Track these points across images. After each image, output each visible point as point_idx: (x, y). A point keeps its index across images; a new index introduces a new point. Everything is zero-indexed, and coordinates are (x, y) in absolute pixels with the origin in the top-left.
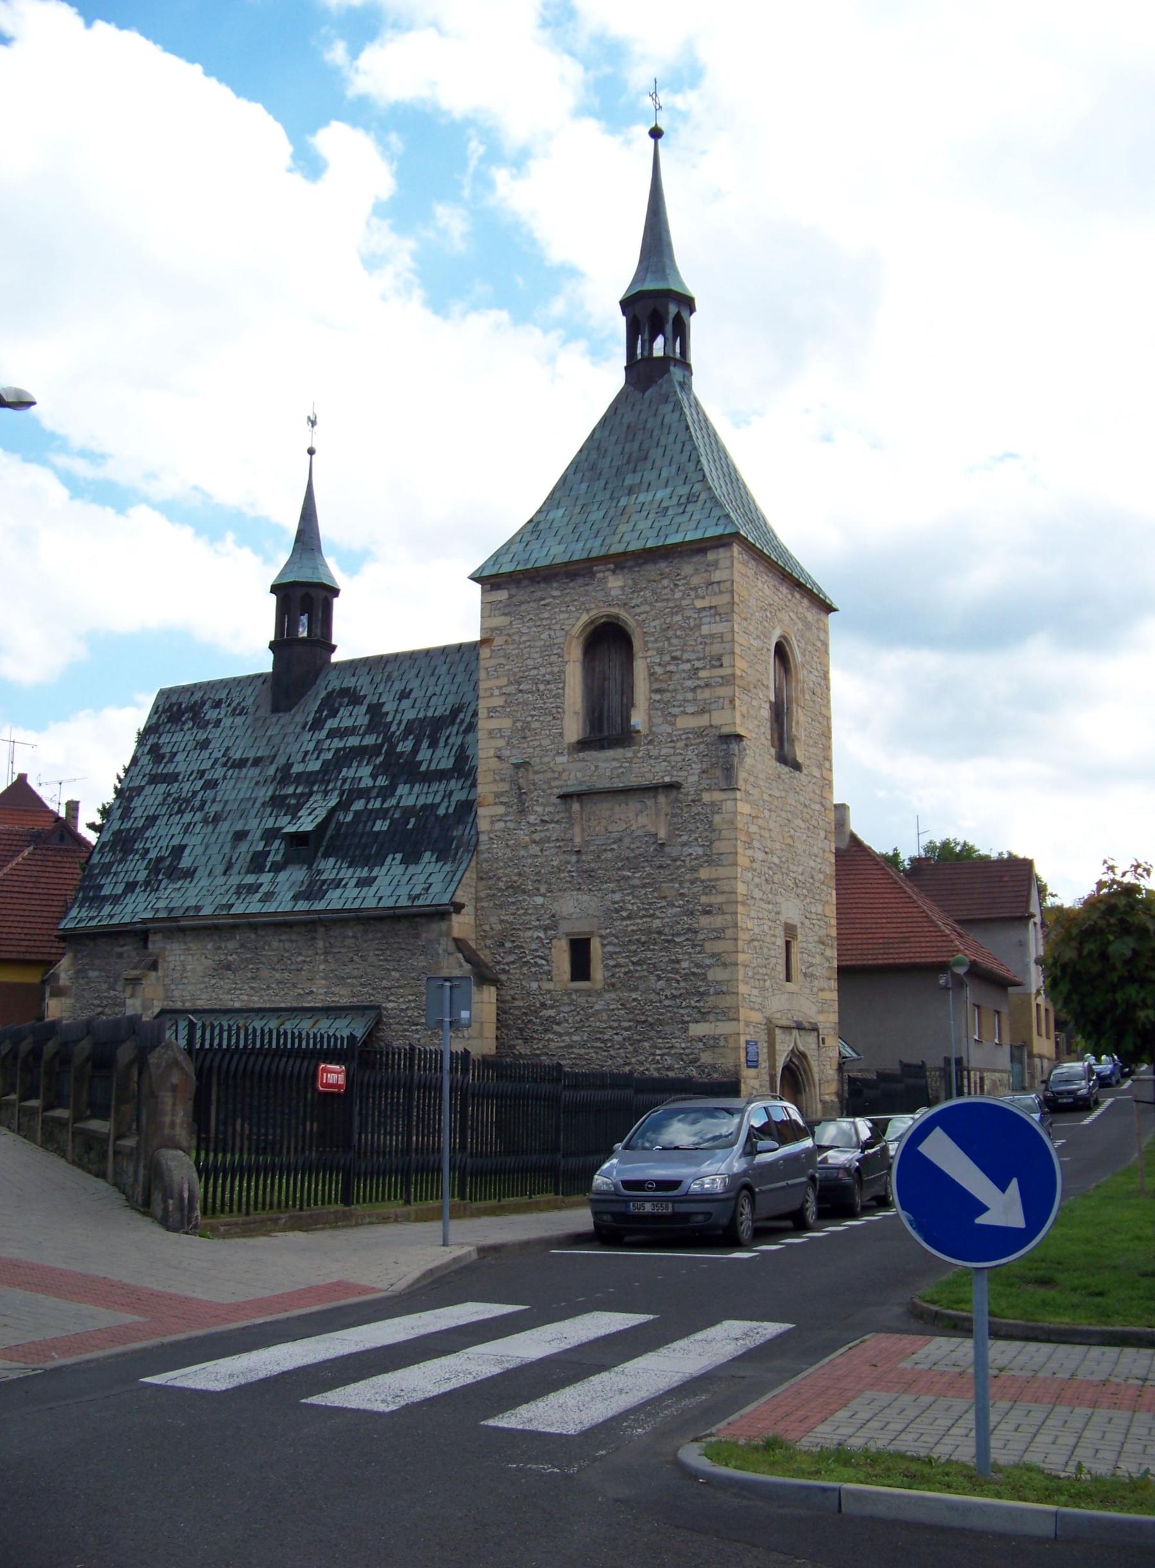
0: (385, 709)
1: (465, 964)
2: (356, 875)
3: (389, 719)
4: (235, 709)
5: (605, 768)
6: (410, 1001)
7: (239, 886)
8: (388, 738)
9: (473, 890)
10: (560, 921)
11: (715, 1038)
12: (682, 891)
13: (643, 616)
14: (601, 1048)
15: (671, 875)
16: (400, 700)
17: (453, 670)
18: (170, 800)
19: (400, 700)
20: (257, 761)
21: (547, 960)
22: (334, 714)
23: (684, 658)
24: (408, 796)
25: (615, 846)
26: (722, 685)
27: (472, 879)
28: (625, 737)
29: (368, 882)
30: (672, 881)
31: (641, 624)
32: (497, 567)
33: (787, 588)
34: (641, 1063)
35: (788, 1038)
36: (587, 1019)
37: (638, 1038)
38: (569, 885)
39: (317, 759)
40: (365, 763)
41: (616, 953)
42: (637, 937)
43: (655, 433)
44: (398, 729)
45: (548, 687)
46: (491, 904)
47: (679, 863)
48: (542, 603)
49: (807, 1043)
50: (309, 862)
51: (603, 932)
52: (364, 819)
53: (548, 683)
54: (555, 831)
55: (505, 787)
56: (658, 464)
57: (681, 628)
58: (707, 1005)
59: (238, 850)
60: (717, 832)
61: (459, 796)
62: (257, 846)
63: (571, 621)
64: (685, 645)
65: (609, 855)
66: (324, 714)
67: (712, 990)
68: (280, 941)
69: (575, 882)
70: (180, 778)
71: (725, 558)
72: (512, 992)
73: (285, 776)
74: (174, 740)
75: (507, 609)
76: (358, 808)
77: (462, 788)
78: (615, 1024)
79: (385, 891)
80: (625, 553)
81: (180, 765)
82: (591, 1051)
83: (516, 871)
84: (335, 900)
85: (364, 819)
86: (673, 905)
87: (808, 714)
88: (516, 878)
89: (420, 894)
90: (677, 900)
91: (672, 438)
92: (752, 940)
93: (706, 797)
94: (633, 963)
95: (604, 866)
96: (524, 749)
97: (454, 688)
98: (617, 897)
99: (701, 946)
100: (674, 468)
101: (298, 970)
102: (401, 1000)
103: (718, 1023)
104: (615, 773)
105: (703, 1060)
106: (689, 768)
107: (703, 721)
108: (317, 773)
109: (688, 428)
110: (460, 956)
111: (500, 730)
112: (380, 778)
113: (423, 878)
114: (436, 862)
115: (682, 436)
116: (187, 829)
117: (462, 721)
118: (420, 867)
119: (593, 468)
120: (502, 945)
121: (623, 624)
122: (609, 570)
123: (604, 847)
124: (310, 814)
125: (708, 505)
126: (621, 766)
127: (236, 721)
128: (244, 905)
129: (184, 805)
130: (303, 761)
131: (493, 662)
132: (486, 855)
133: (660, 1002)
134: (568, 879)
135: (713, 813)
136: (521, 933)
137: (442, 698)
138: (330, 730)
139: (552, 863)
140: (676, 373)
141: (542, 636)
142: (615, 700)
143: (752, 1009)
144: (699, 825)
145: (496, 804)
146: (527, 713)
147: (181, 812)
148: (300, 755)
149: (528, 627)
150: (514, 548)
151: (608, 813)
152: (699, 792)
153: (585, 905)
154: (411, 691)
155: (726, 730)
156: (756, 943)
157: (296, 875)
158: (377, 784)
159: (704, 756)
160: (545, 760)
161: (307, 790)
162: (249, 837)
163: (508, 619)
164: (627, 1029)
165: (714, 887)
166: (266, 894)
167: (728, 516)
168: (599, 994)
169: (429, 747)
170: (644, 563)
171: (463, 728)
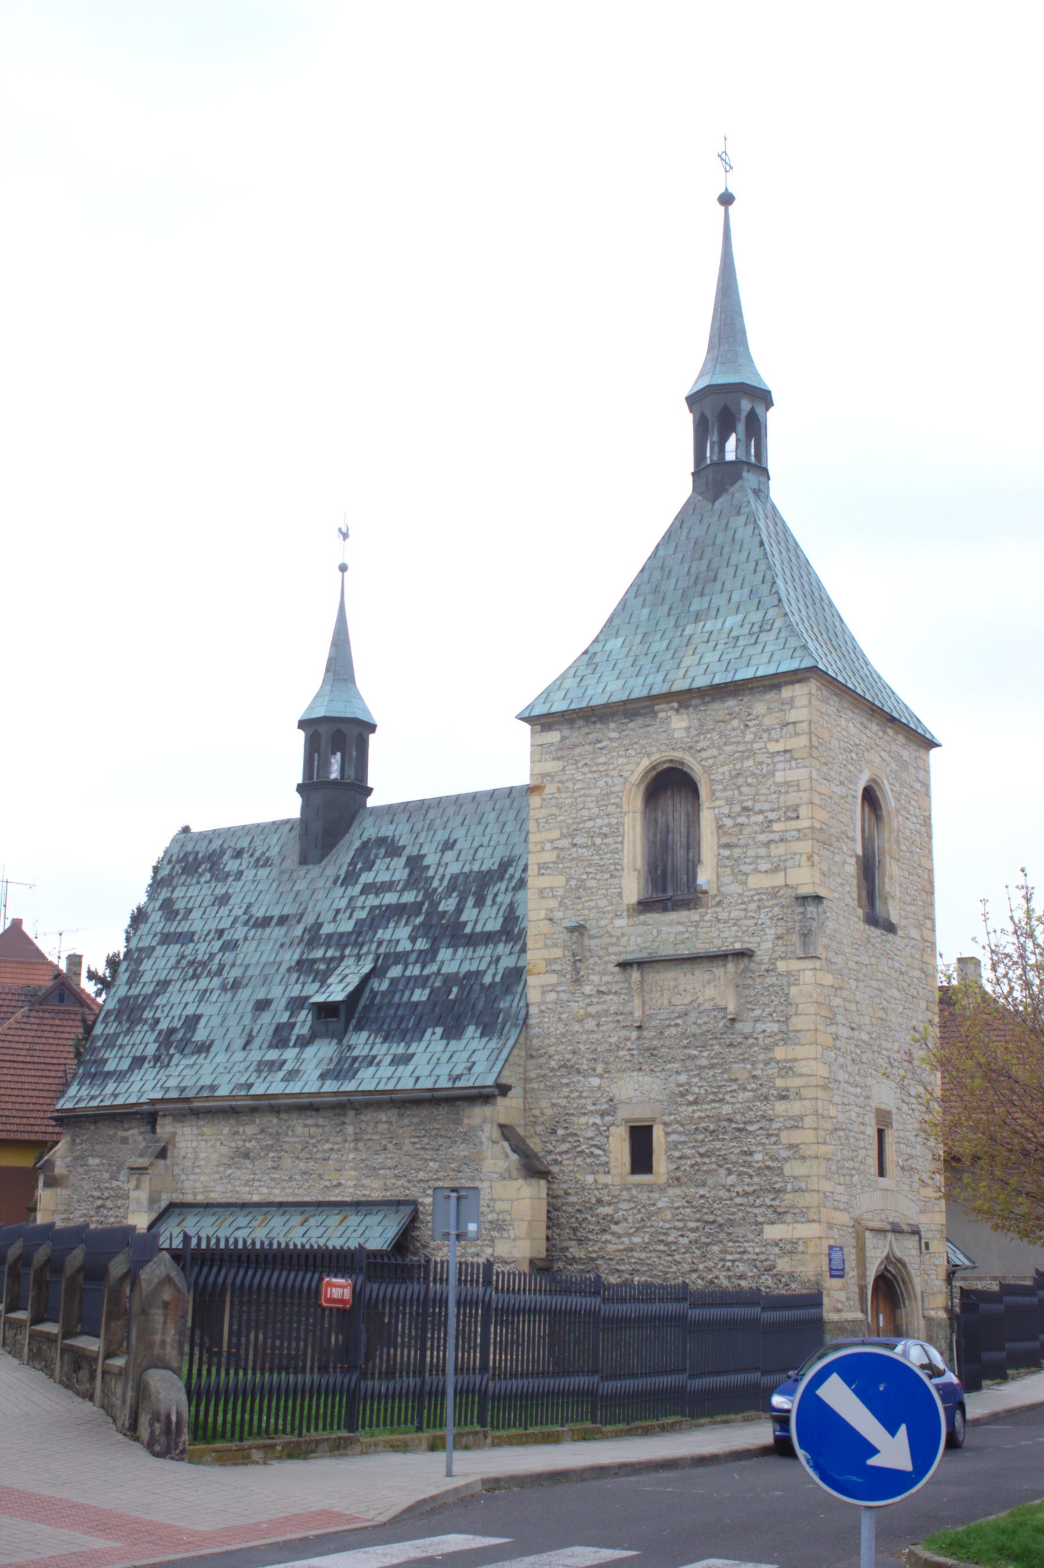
0: (426, 862)
2: (392, 1051)
3: (431, 873)
4: (258, 860)
7: (260, 1063)
8: (429, 894)
9: (521, 1070)
11: (794, 1243)
12: (754, 1073)
13: (711, 761)
14: (664, 1252)
18: (184, 962)
19: (443, 851)
20: (283, 920)
21: (604, 1150)
22: (369, 866)
23: (756, 809)
26: (798, 839)
27: (521, 1057)
29: (406, 1059)
30: (744, 1060)
31: (708, 770)
33: (877, 724)
35: (881, 1242)
37: (707, 1240)
38: (629, 1065)
39: (350, 917)
43: (726, 550)
44: (440, 885)
46: (542, 1086)
47: (751, 1041)
49: (906, 1249)
50: (339, 1036)
51: (667, 1119)
53: (606, 836)
55: (558, 953)
57: (753, 775)
58: (783, 1204)
59: (259, 1022)
61: (508, 962)
63: (630, 767)
64: (757, 794)
65: (673, 1031)
66: (359, 866)
67: (789, 1187)
68: (305, 1126)
69: (635, 1061)
70: (196, 938)
72: (565, 1186)
73: (313, 937)
74: (189, 894)
75: (560, 752)
78: (680, 1225)
81: (196, 923)
82: (654, 1255)
83: (570, 1048)
84: (367, 1080)
85: (401, 987)
86: (745, 1089)
88: (570, 1056)
89: (462, 1075)
90: (749, 1084)
92: (836, 1129)
93: (781, 966)
94: (701, 1155)
95: (667, 1043)
97: (503, 839)
98: (683, 1078)
99: (777, 1135)
100: (746, 591)
101: (325, 1160)
103: (795, 1225)
104: (680, 937)
107: (778, 879)
108: (350, 934)
109: (762, 544)
110: (506, 1144)
111: (552, 888)
112: (420, 940)
113: (465, 1055)
116: (203, 996)
117: (512, 877)
119: (656, 591)
120: (554, 1132)
122: (672, 709)
123: (667, 1022)
124: (341, 981)
125: (783, 634)
127: (259, 873)
129: (200, 969)
131: (544, 812)
132: (536, 1030)
133: (731, 1199)
134: (628, 1058)
135: (789, 985)
136: (575, 1119)
137: (490, 850)
138: (365, 885)
140: (750, 479)
143: (836, 1209)
144: (773, 997)
145: (547, 972)
146: (582, 870)
147: (195, 976)
148: (331, 914)
152: (773, 961)
153: (647, 1087)
154: (455, 841)
156: (841, 1133)
157: (324, 1051)
158: (417, 946)
162: (273, 1007)
163: (561, 763)
164: (694, 1230)
165: (790, 1068)
166: (290, 1072)
167: (805, 647)
168: (662, 1190)
169: (474, 906)
170: (709, 702)
171: (513, 884)
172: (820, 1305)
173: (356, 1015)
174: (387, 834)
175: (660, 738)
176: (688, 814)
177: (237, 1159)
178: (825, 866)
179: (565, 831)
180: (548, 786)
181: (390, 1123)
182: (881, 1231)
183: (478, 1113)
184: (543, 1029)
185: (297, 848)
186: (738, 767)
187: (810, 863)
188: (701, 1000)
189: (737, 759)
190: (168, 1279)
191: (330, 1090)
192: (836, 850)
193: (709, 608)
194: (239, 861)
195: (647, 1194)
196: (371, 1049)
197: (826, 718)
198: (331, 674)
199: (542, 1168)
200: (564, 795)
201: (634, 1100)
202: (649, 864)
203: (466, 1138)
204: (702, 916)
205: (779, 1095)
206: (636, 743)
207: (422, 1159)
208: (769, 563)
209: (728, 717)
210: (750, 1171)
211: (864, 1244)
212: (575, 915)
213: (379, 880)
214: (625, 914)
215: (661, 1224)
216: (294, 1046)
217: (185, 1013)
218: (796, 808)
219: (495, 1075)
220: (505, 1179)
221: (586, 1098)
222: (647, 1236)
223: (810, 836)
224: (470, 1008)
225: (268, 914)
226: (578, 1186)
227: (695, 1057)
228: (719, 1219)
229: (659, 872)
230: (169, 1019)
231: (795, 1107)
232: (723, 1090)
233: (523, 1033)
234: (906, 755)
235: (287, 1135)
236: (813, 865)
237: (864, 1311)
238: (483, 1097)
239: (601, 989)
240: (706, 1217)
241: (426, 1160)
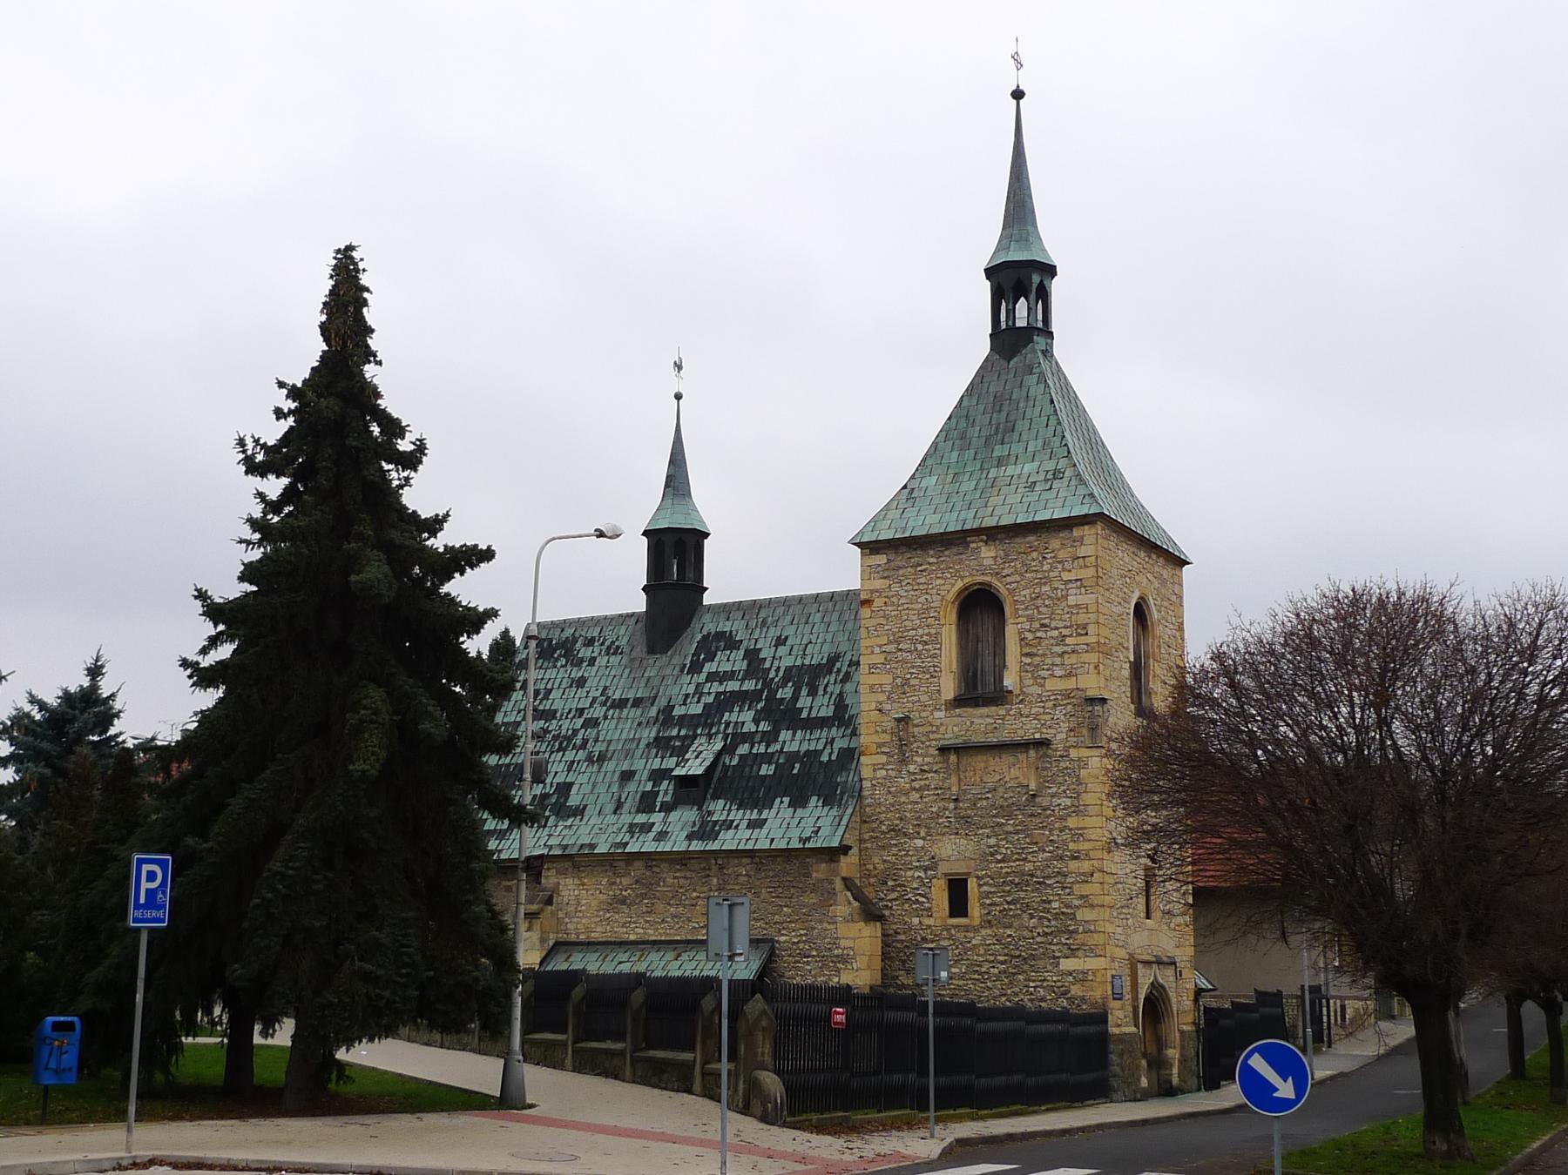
0: (762, 656)
1: (853, 902)
3: (767, 665)
4: (609, 648)
5: (980, 724)
6: (801, 935)
8: (767, 684)
9: (857, 833)
10: (940, 863)
12: (1051, 838)
13: (1014, 585)
14: (978, 980)
16: (776, 646)
19: (776, 646)
20: (637, 702)
21: (927, 898)
23: (1052, 626)
24: (792, 742)
25: (989, 795)
26: (1087, 652)
28: (999, 697)
31: (1012, 592)
32: (876, 533)
33: (1145, 552)
34: (1016, 994)
35: (1148, 971)
37: (1014, 971)
39: (698, 702)
40: (746, 708)
41: (991, 893)
43: (1021, 405)
44: (777, 676)
48: (919, 568)
49: (1166, 977)
50: (699, 803)
52: (750, 762)
53: (926, 643)
54: (933, 779)
55: (887, 738)
56: (1024, 437)
60: (1084, 785)
61: (840, 744)
63: (946, 587)
64: (1053, 614)
66: (702, 657)
67: (1081, 929)
68: (675, 878)
70: (558, 715)
72: (894, 927)
74: (547, 676)
75: (887, 573)
76: (743, 753)
77: (843, 736)
78: (992, 958)
79: (777, 834)
80: (997, 527)
81: (556, 702)
82: (970, 982)
83: (897, 815)
84: (728, 841)
85: (750, 762)
86: (1044, 851)
87: (1164, 666)
88: (898, 822)
90: (1047, 846)
92: (1116, 883)
93: (1074, 753)
94: (1008, 903)
95: (979, 813)
96: (903, 703)
98: (992, 841)
99: (1070, 888)
100: (1040, 442)
102: (793, 934)
103: (1086, 959)
105: (1073, 993)
106: (1057, 726)
107: (1070, 684)
109: (1052, 402)
110: (849, 894)
112: (763, 723)
113: (812, 821)
117: (839, 670)
119: (963, 437)
121: (996, 592)
122: (982, 541)
123: (979, 796)
124: (697, 757)
125: (1073, 483)
126: (995, 723)
128: (638, 844)
130: (685, 704)
131: (874, 622)
132: (869, 800)
133: (1033, 938)
134: (947, 824)
137: (819, 646)
140: (1040, 341)
142: (988, 661)
143: (1117, 946)
144: (1067, 778)
145: (878, 753)
149: (906, 591)
150: (891, 515)
151: (983, 765)
152: (1067, 749)
153: (963, 848)
154: (787, 638)
155: (1090, 693)
156: (1120, 886)
157: (685, 816)
158: (760, 729)
160: (924, 714)
161: (691, 733)
162: (637, 778)
163: (887, 582)
164: (1002, 963)
165: (1081, 835)
166: (660, 833)
167: (1092, 495)
168: (976, 930)
172: (1107, 1022)
173: (713, 786)
178: (1107, 673)
182: (1147, 963)
187: (1097, 671)
188: (1007, 779)
189: (1036, 584)
190: (764, 1012)
192: (1115, 659)
196: (728, 815)
197: (1108, 552)
199: (878, 913)
200: (890, 608)
201: (952, 858)
206: (951, 568)
207: (776, 906)
208: (1059, 419)
212: (900, 707)
216: (659, 811)
218: (1085, 627)
220: (848, 921)
221: (911, 856)
222: (964, 967)
223: (1097, 649)
228: (1023, 954)
231: (1086, 866)
232: (1025, 852)
234: (1165, 573)
235: (659, 885)
237: (1136, 1026)
238: (833, 854)
239: (923, 768)
241: (781, 906)
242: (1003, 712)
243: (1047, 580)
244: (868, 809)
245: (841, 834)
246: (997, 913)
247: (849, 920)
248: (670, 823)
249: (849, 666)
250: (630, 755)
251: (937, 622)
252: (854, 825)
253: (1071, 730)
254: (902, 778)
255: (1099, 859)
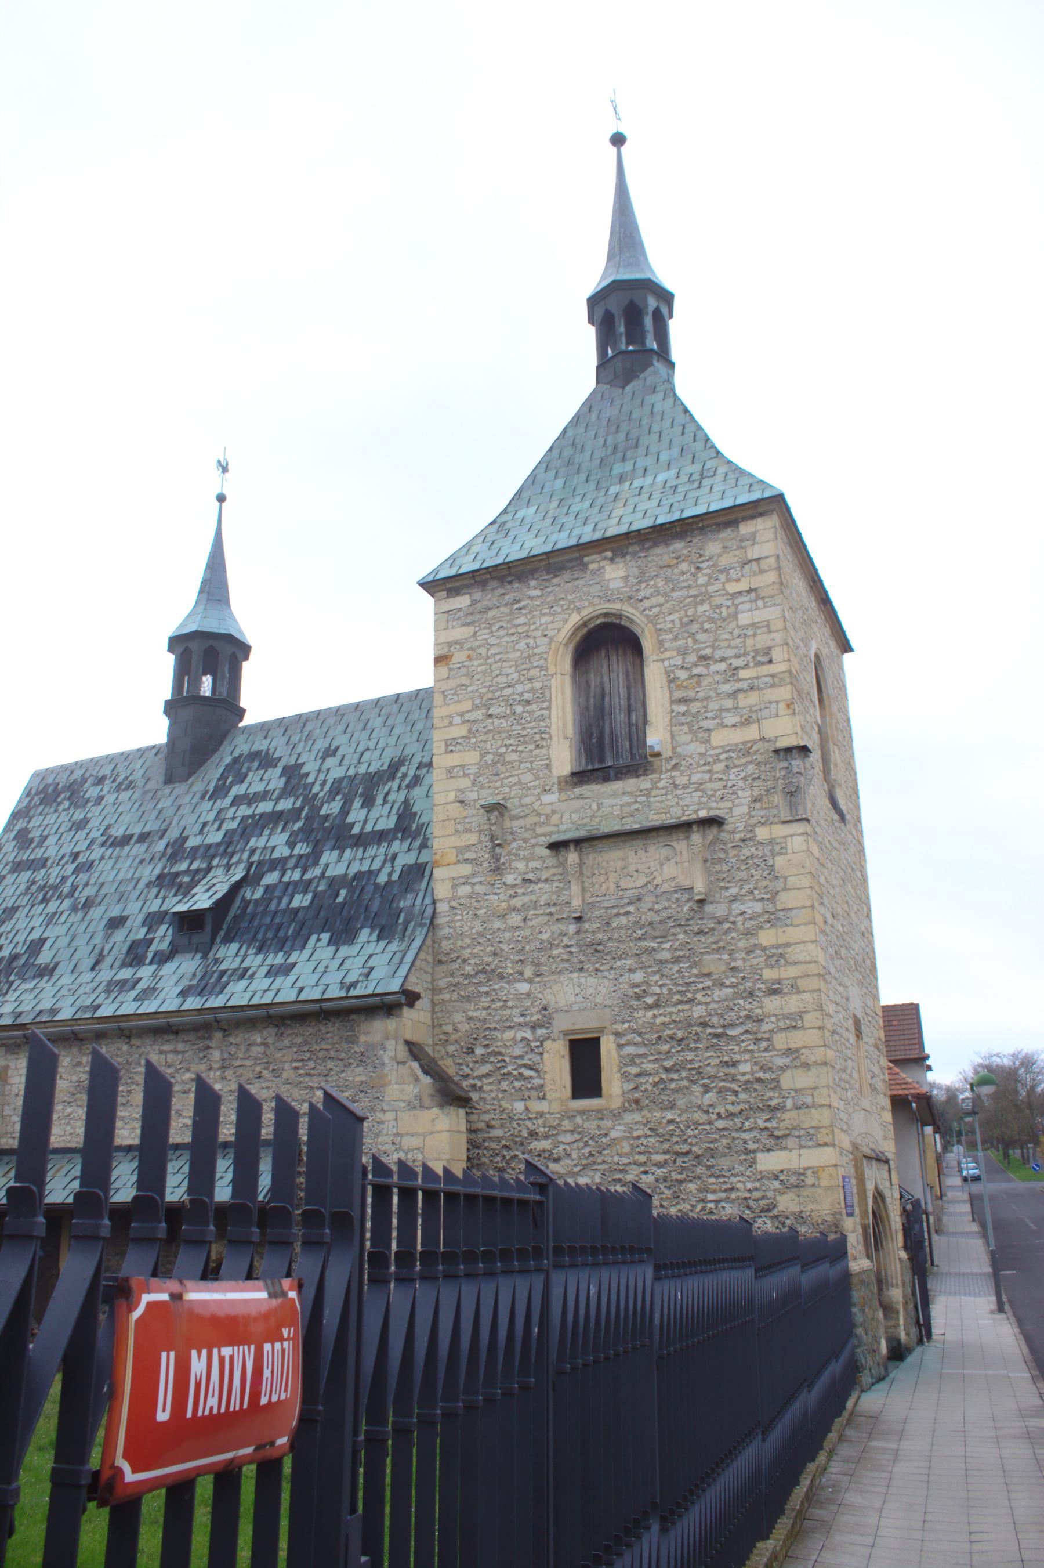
0: (304, 770)
2: (269, 961)
3: (310, 779)
4: (120, 784)
5: (612, 806)
7: (110, 983)
8: (310, 800)
11: (801, 1174)
12: (733, 964)
13: (656, 610)
15: (714, 943)
17: (390, 722)
18: (34, 888)
19: (323, 759)
20: (143, 837)
21: (537, 1071)
22: (241, 779)
23: (717, 657)
25: (631, 908)
26: (773, 686)
27: (428, 962)
29: (287, 969)
30: (718, 950)
31: (653, 620)
36: (600, 1153)
37: (679, 1177)
38: (567, 965)
42: (668, 1032)
43: (644, 422)
44: (322, 790)
45: (528, 708)
46: (455, 996)
47: (726, 926)
50: (204, 950)
51: (619, 1027)
53: (528, 702)
55: (472, 838)
56: (653, 449)
57: (710, 620)
58: (782, 1125)
59: (112, 940)
60: (782, 880)
61: (410, 859)
62: (137, 934)
63: (556, 625)
64: (716, 640)
65: (623, 920)
66: (230, 779)
67: (789, 1103)
68: (161, 1052)
69: (576, 960)
70: (49, 863)
71: (765, 529)
72: (487, 1117)
73: (177, 850)
74: (45, 823)
75: (470, 617)
77: (409, 850)
78: (642, 1158)
80: (628, 534)
81: (51, 849)
83: (489, 949)
84: (238, 994)
85: (277, 893)
86: (722, 985)
88: (490, 959)
89: (357, 982)
90: (727, 978)
91: (667, 423)
94: (667, 1070)
95: (616, 936)
96: (497, 788)
97: (392, 741)
98: (638, 977)
99: (768, 1039)
100: (676, 451)
101: (184, 1092)
103: (803, 1151)
104: (626, 810)
105: (781, 1207)
106: (733, 797)
107: (751, 733)
108: (218, 845)
110: (415, 1065)
111: (462, 766)
112: (299, 845)
114: (378, 941)
115: (681, 418)
116: (51, 919)
117: (405, 775)
118: (355, 949)
120: (471, 1051)
121: (627, 624)
122: (605, 558)
123: (615, 911)
124: (207, 890)
125: (731, 476)
126: (636, 802)
127: (120, 797)
129: (50, 893)
132: (446, 931)
133: (710, 1123)
134: (565, 957)
135: (773, 855)
136: (497, 1034)
137: (377, 753)
138: (236, 797)
139: (540, 936)
140: (658, 365)
141: (517, 647)
144: (753, 871)
146: (500, 743)
147: (45, 900)
148: (198, 827)
153: (591, 991)
154: (337, 748)
155: (783, 743)
157: (188, 965)
158: (296, 851)
159: (754, 779)
162: (128, 924)
163: (471, 629)
164: (660, 1165)
165: (781, 955)
166: (144, 991)
168: (616, 1115)
169: (362, 807)
170: (650, 547)
171: (407, 781)
173: (225, 927)
174: (261, 748)
175: (592, 590)
176: (627, 674)
177: (79, 1095)
179: (477, 701)
180: (456, 654)
181: (266, 1045)
183: (378, 1029)
184: (455, 928)
185: (162, 770)
186: (689, 613)
187: (790, 711)
189: (688, 604)
191: (192, 1008)
193: (634, 469)
194: (100, 787)
195: (596, 1122)
196: (242, 962)
198: (205, 595)
199: (461, 1093)
200: (476, 663)
201: (575, 1007)
202: (581, 733)
203: (363, 1059)
204: (655, 783)
205: (768, 988)
209: (675, 561)
210: (734, 1086)
211: (863, 1173)
212: (492, 794)
213: (251, 791)
214: (555, 788)
215: (616, 1159)
216: (151, 963)
217: (31, 937)
218: (767, 651)
219: (401, 980)
222: (598, 1174)
224: (362, 910)
225: (127, 833)
226: (505, 1116)
227: (654, 949)
228: (694, 1149)
229: (594, 741)
230: (12, 945)
231: (792, 1003)
232: (692, 988)
233: (430, 934)
236: (794, 713)
239: (527, 877)
240: (677, 1148)
242: (648, 785)
243: (706, 597)
244: (444, 943)
245: (404, 974)
246: (650, 1088)
247: (417, 1105)
248: (162, 977)
249: (418, 768)
250: (124, 898)
251: (543, 673)
252: (424, 965)
253: (755, 801)
254: (496, 894)
255: (815, 991)
